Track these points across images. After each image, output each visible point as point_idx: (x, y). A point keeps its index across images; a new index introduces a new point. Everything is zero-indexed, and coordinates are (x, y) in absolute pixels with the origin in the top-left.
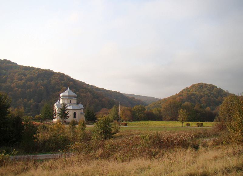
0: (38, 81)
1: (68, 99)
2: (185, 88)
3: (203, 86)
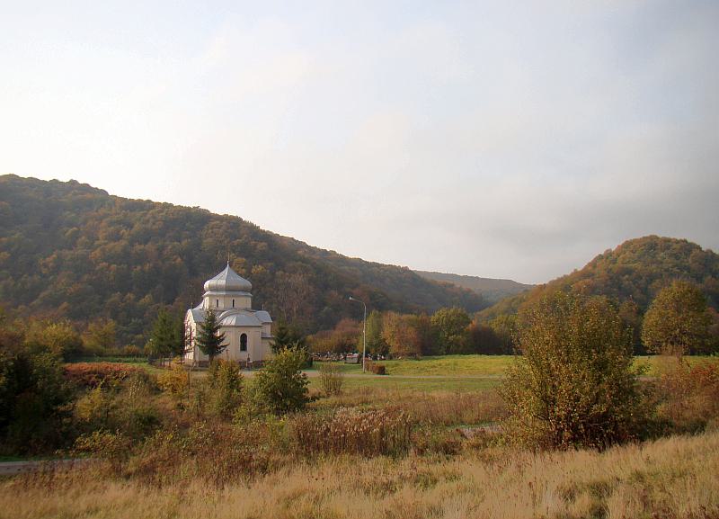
0: (164, 241)
1: (224, 296)
2: (602, 253)
3: (656, 245)
